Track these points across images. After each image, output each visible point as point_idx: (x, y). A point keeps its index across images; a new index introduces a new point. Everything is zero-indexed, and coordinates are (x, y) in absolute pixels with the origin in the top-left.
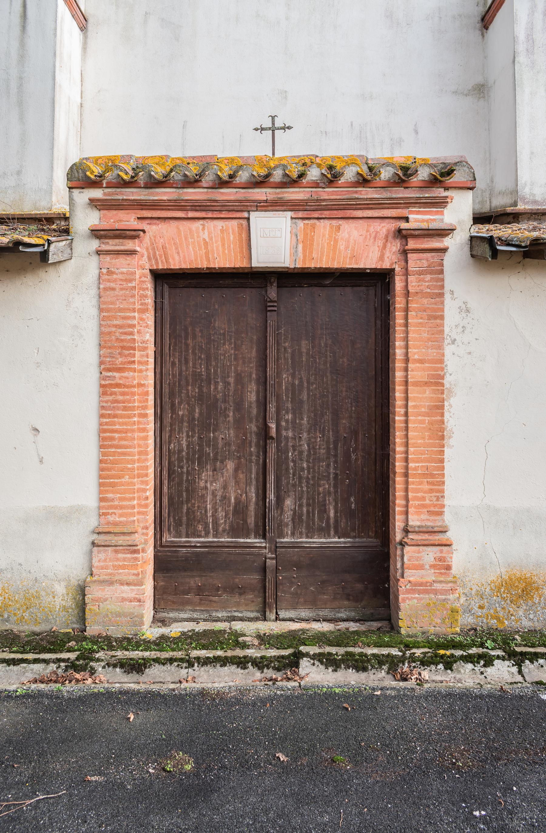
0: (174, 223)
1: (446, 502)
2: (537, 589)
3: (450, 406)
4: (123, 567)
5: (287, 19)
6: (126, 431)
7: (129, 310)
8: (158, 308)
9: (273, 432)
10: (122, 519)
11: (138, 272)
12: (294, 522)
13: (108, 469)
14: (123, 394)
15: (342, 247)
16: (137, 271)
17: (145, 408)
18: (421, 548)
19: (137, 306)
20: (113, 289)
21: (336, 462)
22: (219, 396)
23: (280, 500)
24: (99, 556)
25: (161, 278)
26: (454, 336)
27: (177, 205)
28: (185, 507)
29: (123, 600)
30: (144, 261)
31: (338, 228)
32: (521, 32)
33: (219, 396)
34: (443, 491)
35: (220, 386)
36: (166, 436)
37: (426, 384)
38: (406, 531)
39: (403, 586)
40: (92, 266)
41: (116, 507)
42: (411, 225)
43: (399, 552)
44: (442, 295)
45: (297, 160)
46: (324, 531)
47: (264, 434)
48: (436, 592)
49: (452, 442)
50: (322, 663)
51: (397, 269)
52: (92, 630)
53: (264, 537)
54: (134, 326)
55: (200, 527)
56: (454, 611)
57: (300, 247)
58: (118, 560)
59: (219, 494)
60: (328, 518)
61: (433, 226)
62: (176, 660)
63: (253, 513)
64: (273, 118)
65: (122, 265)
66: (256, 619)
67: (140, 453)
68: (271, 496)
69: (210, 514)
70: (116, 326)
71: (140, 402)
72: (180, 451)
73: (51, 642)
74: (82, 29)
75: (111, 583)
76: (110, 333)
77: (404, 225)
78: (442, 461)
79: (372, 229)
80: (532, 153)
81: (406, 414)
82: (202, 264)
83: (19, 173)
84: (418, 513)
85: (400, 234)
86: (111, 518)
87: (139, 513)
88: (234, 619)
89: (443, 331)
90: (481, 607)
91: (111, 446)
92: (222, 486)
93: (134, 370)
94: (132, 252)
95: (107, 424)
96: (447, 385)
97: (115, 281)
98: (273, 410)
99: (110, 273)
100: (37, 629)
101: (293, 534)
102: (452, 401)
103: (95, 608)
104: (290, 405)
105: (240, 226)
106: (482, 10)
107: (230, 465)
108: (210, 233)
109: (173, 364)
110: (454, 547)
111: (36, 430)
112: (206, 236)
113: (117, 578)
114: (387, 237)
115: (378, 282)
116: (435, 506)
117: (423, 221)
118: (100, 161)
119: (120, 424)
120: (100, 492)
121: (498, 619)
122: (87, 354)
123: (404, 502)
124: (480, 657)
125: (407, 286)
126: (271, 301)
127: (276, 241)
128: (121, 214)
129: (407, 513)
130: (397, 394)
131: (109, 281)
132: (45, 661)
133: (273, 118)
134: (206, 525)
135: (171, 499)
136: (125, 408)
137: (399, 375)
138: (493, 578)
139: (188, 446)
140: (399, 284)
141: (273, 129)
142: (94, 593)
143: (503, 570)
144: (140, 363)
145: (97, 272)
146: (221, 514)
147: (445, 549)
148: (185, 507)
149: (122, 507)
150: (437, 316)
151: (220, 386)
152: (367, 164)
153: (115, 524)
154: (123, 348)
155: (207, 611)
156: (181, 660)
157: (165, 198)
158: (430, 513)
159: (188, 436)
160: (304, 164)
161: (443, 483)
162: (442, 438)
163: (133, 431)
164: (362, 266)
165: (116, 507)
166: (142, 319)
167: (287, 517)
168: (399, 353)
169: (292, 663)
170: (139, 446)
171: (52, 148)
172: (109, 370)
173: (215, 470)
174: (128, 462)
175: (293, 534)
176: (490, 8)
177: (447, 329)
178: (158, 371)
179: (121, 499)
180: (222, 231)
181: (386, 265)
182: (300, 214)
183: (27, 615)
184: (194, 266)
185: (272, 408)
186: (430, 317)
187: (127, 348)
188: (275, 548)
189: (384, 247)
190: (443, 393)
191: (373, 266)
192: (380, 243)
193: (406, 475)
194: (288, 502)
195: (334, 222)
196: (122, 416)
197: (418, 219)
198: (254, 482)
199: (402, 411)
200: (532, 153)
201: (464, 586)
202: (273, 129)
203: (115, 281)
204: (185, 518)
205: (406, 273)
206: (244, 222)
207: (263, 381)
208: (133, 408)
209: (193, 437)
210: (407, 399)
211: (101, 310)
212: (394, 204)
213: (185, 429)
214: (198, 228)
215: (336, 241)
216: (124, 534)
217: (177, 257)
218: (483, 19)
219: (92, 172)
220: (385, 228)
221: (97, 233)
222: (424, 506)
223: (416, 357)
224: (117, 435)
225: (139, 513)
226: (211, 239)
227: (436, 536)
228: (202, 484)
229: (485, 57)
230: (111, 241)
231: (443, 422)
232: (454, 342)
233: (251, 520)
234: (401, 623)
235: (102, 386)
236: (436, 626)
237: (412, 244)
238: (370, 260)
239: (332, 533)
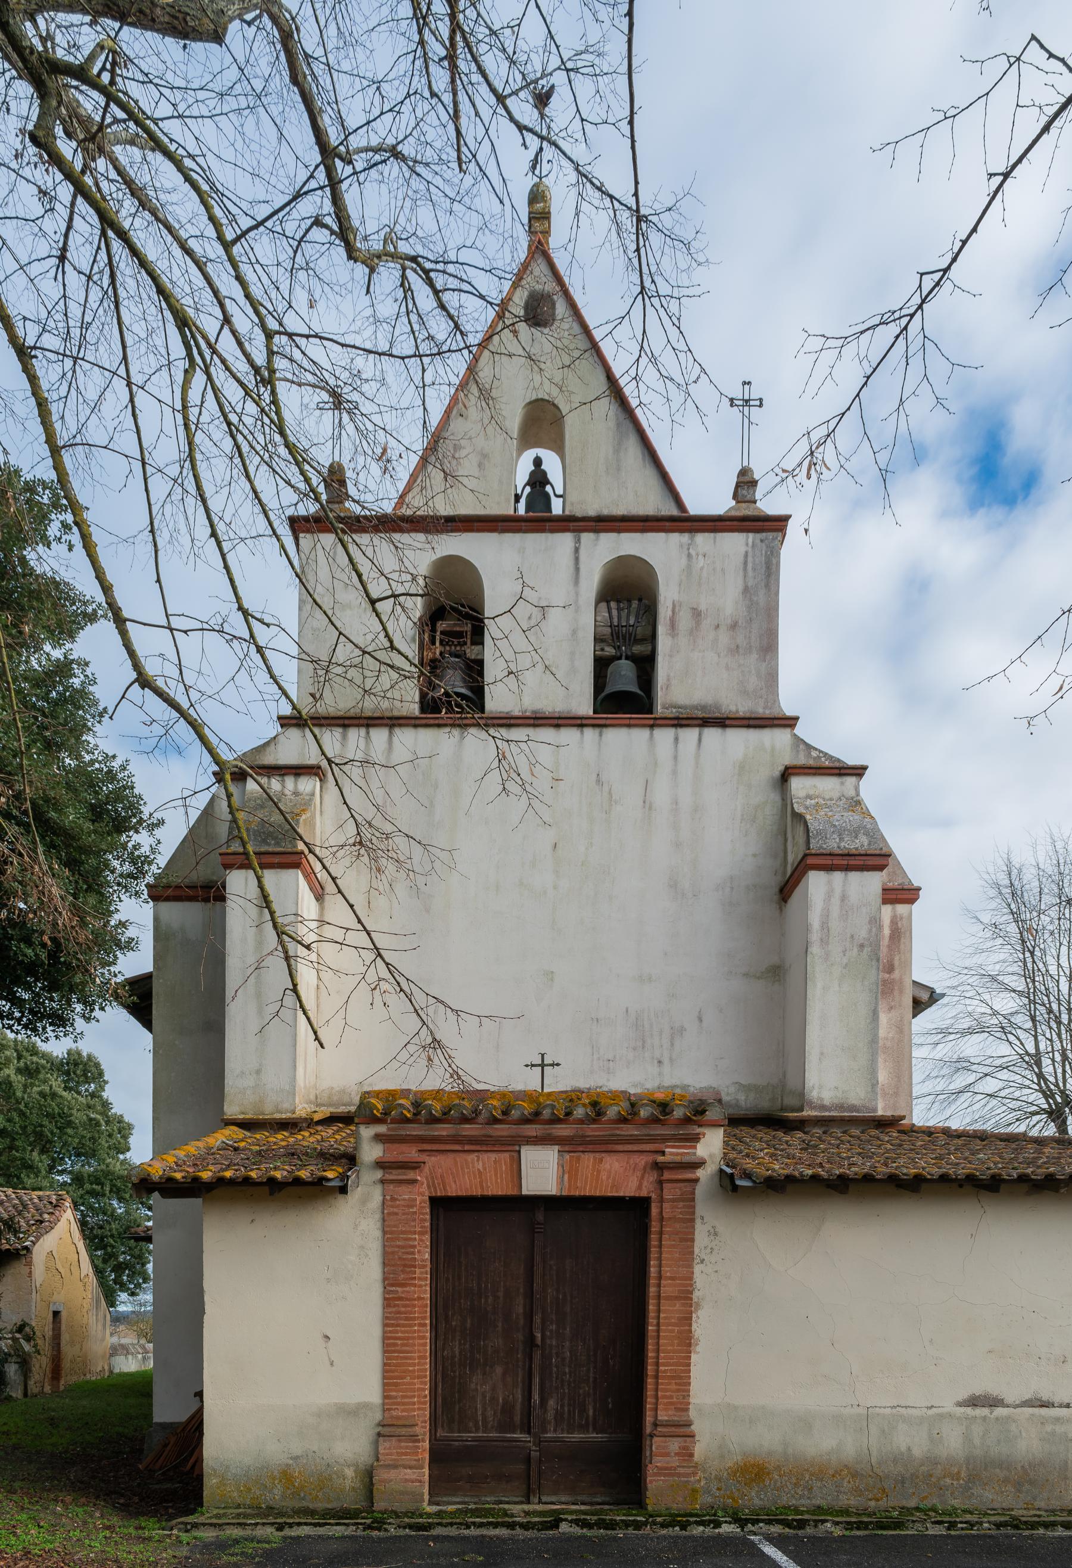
0: (451, 1155)
1: (691, 1400)
2: (768, 1474)
3: (698, 1317)
4: (406, 1454)
5: (555, 888)
6: (408, 1338)
7: (411, 1233)
8: (434, 1230)
9: (539, 1341)
10: (404, 1414)
11: (419, 1199)
12: (556, 1420)
13: (393, 1371)
14: (405, 1306)
15: (604, 1177)
16: (419, 1196)
17: (425, 1318)
18: (668, 1439)
19: (418, 1229)
20: (396, 1214)
21: (595, 1367)
22: (489, 1308)
23: (543, 1401)
24: (384, 1446)
25: (439, 1204)
26: (703, 1256)
27: (455, 1139)
28: (457, 1407)
29: (406, 1481)
30: (424, 1189)
31: (601, 1160)
32: (815, 919)
33: (489, 1308)
34: (689, 1391)
35: (490, 1300)
36: (440, 1344)
37: (676, 1298)
38: (655, 1425)
39: (650, 1470)
40: (377, 1196)
41: (398, 1404)
42: (667, 1158)
43: (648, 1443)
44: (693, 1220)
45: (564, 1096)
46: (583, 1428)
47: (530, 1342)
48: (679, 1475)
49: (698, 1349)
50: (578, 1525)
51: (653, 1196)
52: (379, 1505)
53: (529, 1433)
54: (414, 1247)
55: (471, 1424)
56: (694, 1491)
57: (566, 1176)
58: (401, 1448)
59: (488, 1396)
60: (588, 1416)
61: (686, 1159)
62: (456, 1524)
63: (519, 1412)
64: (543, 1055)
65: (405, 1193)
66: (522, 1503)
67: (420, 1357)
68: (536, 1397)
69: (479, 1413)
70: (399, 1246)
71: (420, 1313)
72: (453, 1357)
73: (343, 1515)
74: (317, 899)
75: (395, 1467)
76: (393, 1253)
77: (661, 1159)
78: (689, 1365)
79: (632, 1161)
80: (822, 1054)
81: (658, 1324)
82: (477, 1192)
83: (258, 1072)
84: (666, 1410)
85: (658, 1167)
86: (394, 1413)
87: (419, 1409)
88: (501, 1502)
89: (693, 1252)
90: (718, 1489)
91: (394, 1352)
92: (490, 1389)
93: (415, 1285)
94: (415, 1181)
95: (390, 1332)
96: (695, 1299)
97: (398, 1206)
98: (539, 1321)
99: (393, 1199)
100: (329, 1506)
101: (555, 1431)
102: (700, 1313)
103: (382, 1488)
104: (554, 1317)
105: (512, 1158)
106: (779, 880)
107: (499, 1370)
108: (484, 1164)
109: (447, 1279)
110: (697, 1438)
111: (327, 1337)
112: (480, 1167)
113: (400, 1463)
114: (645, 1168)
115: (639, 1206)
116: (681, 1403)
117: (677, 1154)
118: (380, 1096)
119: (402, 1332)
120: (384, 1391)
121: (733, 1499)
122: (372, 1270)
123: (654, 1401)
124: (710, 1522)
125: (661, 1212)
126: (539, 1224)
127: (542, 1171)
128: (404, 1147)
129: (656, 1409)
130: (651, 1307)
131: (392, 1207)
132: (344, 1524)
133: (543, 1055)
134: (476, 1422)
135: (444, 1399)
136: (407, 1319)
137: (652, 1290)
138: (730, 1464)
139: (460, 1353)
140: (654, 1211)
141: (543, 1066)
142: (380, 1475)
143: (739, 1458)
144: (420, 1279)
145: (381, 1198)
146: (490, 1413)
147: (688, 1439)
148: (457, 1407)
149: (404, 1404)
150: (688, 1239)
151: (490, 1300)
152: (629, 1100)
153: (398, 1418)
154: (405, 1266)
155: (477, 1496)
156: (461, 1524)
157: (444, 1133)
158: (677, 1409)
159: (460, 1344)
160: (571, 1100)
161: (689, 1384)
162: (690, 1345)
163: (414, 1338)
164: (621, 1194)
165: (398, 1404)
166: (422, 1240)
167: (550, 1415)
168: (653, 1271)
169: (555, 1525)
170: (419, 1351)
171: (295, 1045)
172: (392, 1285)
173: (484, 1374)
174: (410, 1365)
175: (555, 1431)
176: (788, 881)
177: (696, 1250)
178: (434, 1286)
179: (403, 1397)
180: (495, 1162)
181: (644, 1193)
182: (567, 1148)
183: (320, 1494)
184: (469, 1194)
185: (537, 1319)
186: (682, 1240)
187: (409, 1265)
188: (539, 1442)
189: (643, 1177)
190: (691, 1306)
191: (632, 1194)
192: (639, 1174)
193: (657, 1377)
194: (551, 1403)
195: (597, 1155)
196: (404, 1326)
197: (673, 1153)
198: (520, 1385)
199: (655, 1322)
200: (822, 1054)
201: (704, 1471)
202: (543, 1066)
203: (398, 1206)
204: (457, 1416)
205: (661, 1200)
206: (515, 1155)
207: (530, 1294)
208: (414, 1319)
209: (465, 1344)
210: (659, 1311)
211: (384, 1232)
212: (652, 1140)
213: (458, 1338)
214: (473, 1160)
215: (599, 1172)
216: (405, 1426)
217: (454, 1186)
218: (781, 890)
219: (378, 1110)
220: (642, 1160)
221: (380, 1164)
222: (672, 1403)
223: (668, 1274)
224: (399, 1342)
225: (419, 1409)
226: (485, 1169)
227: (682, 1429)
228: (473, 1386)
229: (783, 935)
230: (394, 1172)
231: (690, 1331)
232: (702, 1261)
233: (517, 1418)
234: (648, 1501)
235: (385, 1299)
236: (678, 1504)
237: (667, 1175)
238: (629, 1189)
239: (591, 1429)
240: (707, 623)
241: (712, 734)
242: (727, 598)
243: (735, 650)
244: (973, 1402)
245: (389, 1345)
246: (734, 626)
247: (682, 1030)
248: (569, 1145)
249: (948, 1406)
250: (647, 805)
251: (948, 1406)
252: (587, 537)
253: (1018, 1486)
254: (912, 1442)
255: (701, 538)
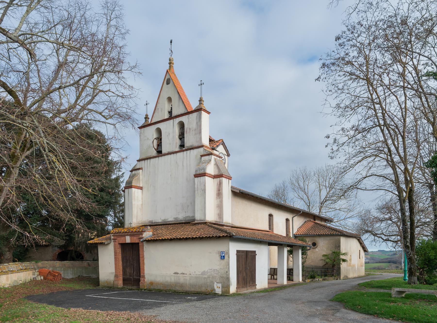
27: (119, 235)
227: (144, 277)
240: (191, 130)
241: (192, 151)
242: (194, 125)
243: (195, 134)
244: (175, 273)
245: (116, 264)
246: (195, 130)
247: (189, 206)
248: (131, 235)
249: (172, 274)
250: (183, 166)
251: (172, 274)
252: (175, 119)
253: (181, 287)
254: (168, 279)
255: (190, 115)
